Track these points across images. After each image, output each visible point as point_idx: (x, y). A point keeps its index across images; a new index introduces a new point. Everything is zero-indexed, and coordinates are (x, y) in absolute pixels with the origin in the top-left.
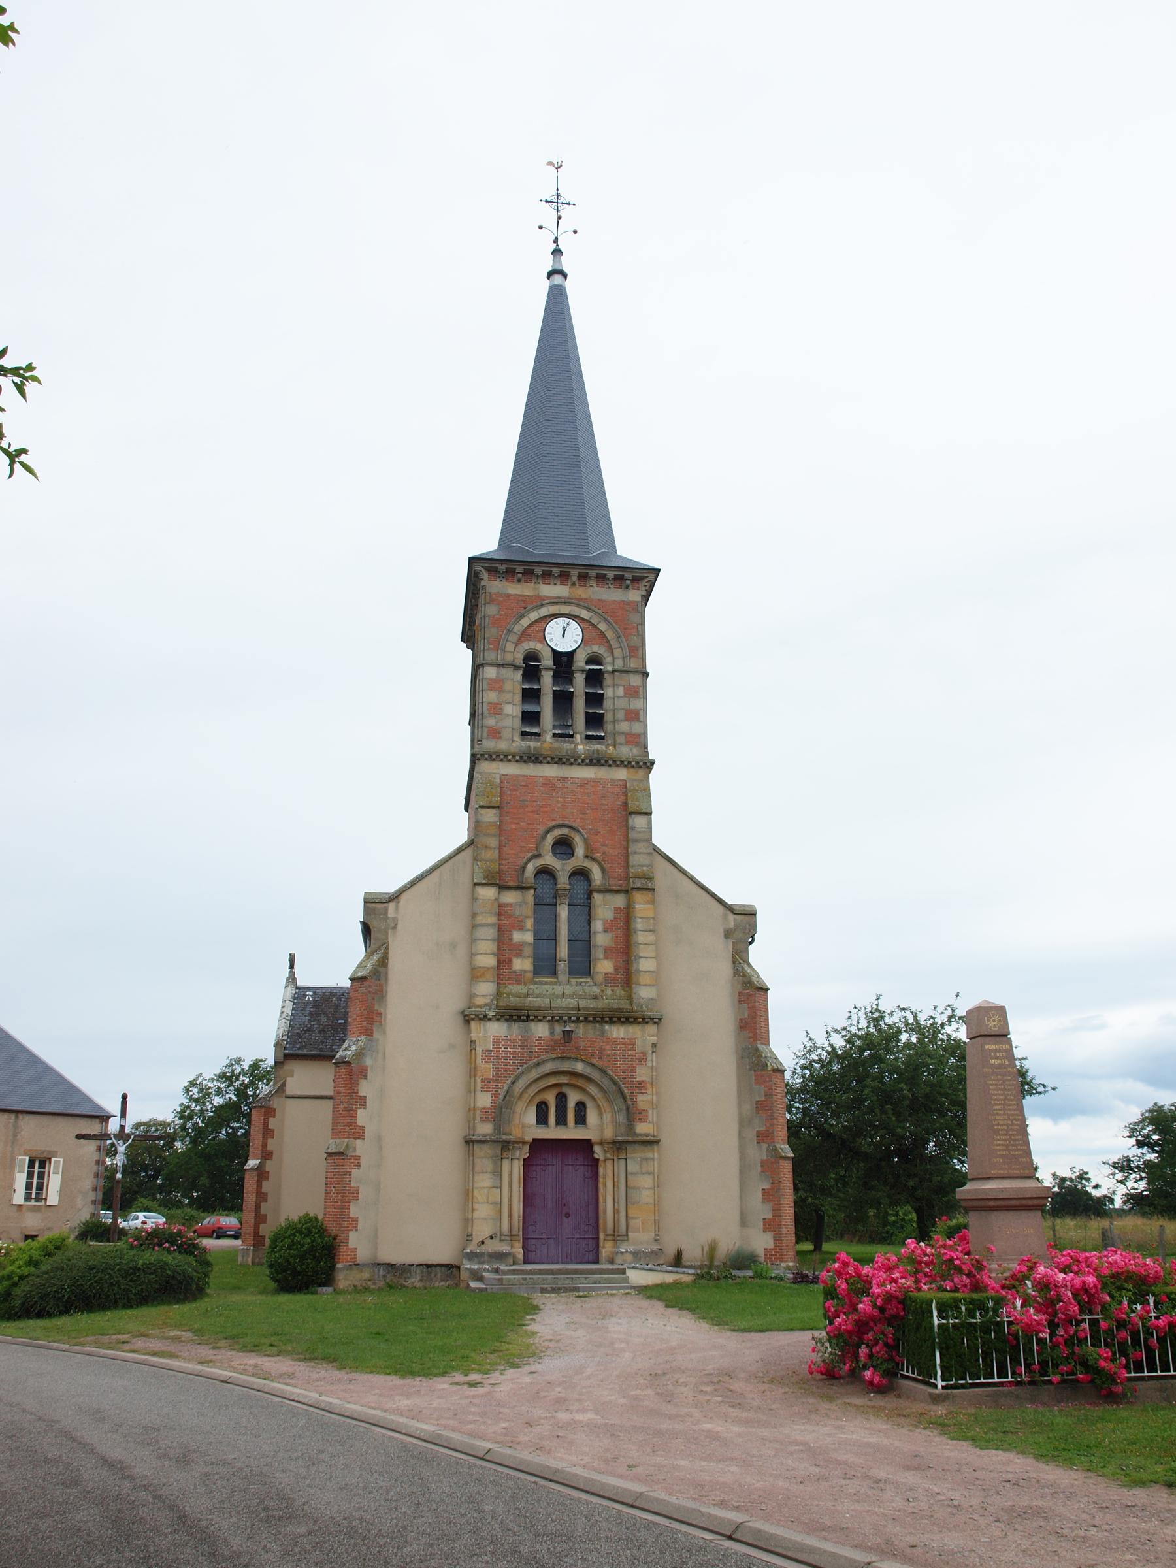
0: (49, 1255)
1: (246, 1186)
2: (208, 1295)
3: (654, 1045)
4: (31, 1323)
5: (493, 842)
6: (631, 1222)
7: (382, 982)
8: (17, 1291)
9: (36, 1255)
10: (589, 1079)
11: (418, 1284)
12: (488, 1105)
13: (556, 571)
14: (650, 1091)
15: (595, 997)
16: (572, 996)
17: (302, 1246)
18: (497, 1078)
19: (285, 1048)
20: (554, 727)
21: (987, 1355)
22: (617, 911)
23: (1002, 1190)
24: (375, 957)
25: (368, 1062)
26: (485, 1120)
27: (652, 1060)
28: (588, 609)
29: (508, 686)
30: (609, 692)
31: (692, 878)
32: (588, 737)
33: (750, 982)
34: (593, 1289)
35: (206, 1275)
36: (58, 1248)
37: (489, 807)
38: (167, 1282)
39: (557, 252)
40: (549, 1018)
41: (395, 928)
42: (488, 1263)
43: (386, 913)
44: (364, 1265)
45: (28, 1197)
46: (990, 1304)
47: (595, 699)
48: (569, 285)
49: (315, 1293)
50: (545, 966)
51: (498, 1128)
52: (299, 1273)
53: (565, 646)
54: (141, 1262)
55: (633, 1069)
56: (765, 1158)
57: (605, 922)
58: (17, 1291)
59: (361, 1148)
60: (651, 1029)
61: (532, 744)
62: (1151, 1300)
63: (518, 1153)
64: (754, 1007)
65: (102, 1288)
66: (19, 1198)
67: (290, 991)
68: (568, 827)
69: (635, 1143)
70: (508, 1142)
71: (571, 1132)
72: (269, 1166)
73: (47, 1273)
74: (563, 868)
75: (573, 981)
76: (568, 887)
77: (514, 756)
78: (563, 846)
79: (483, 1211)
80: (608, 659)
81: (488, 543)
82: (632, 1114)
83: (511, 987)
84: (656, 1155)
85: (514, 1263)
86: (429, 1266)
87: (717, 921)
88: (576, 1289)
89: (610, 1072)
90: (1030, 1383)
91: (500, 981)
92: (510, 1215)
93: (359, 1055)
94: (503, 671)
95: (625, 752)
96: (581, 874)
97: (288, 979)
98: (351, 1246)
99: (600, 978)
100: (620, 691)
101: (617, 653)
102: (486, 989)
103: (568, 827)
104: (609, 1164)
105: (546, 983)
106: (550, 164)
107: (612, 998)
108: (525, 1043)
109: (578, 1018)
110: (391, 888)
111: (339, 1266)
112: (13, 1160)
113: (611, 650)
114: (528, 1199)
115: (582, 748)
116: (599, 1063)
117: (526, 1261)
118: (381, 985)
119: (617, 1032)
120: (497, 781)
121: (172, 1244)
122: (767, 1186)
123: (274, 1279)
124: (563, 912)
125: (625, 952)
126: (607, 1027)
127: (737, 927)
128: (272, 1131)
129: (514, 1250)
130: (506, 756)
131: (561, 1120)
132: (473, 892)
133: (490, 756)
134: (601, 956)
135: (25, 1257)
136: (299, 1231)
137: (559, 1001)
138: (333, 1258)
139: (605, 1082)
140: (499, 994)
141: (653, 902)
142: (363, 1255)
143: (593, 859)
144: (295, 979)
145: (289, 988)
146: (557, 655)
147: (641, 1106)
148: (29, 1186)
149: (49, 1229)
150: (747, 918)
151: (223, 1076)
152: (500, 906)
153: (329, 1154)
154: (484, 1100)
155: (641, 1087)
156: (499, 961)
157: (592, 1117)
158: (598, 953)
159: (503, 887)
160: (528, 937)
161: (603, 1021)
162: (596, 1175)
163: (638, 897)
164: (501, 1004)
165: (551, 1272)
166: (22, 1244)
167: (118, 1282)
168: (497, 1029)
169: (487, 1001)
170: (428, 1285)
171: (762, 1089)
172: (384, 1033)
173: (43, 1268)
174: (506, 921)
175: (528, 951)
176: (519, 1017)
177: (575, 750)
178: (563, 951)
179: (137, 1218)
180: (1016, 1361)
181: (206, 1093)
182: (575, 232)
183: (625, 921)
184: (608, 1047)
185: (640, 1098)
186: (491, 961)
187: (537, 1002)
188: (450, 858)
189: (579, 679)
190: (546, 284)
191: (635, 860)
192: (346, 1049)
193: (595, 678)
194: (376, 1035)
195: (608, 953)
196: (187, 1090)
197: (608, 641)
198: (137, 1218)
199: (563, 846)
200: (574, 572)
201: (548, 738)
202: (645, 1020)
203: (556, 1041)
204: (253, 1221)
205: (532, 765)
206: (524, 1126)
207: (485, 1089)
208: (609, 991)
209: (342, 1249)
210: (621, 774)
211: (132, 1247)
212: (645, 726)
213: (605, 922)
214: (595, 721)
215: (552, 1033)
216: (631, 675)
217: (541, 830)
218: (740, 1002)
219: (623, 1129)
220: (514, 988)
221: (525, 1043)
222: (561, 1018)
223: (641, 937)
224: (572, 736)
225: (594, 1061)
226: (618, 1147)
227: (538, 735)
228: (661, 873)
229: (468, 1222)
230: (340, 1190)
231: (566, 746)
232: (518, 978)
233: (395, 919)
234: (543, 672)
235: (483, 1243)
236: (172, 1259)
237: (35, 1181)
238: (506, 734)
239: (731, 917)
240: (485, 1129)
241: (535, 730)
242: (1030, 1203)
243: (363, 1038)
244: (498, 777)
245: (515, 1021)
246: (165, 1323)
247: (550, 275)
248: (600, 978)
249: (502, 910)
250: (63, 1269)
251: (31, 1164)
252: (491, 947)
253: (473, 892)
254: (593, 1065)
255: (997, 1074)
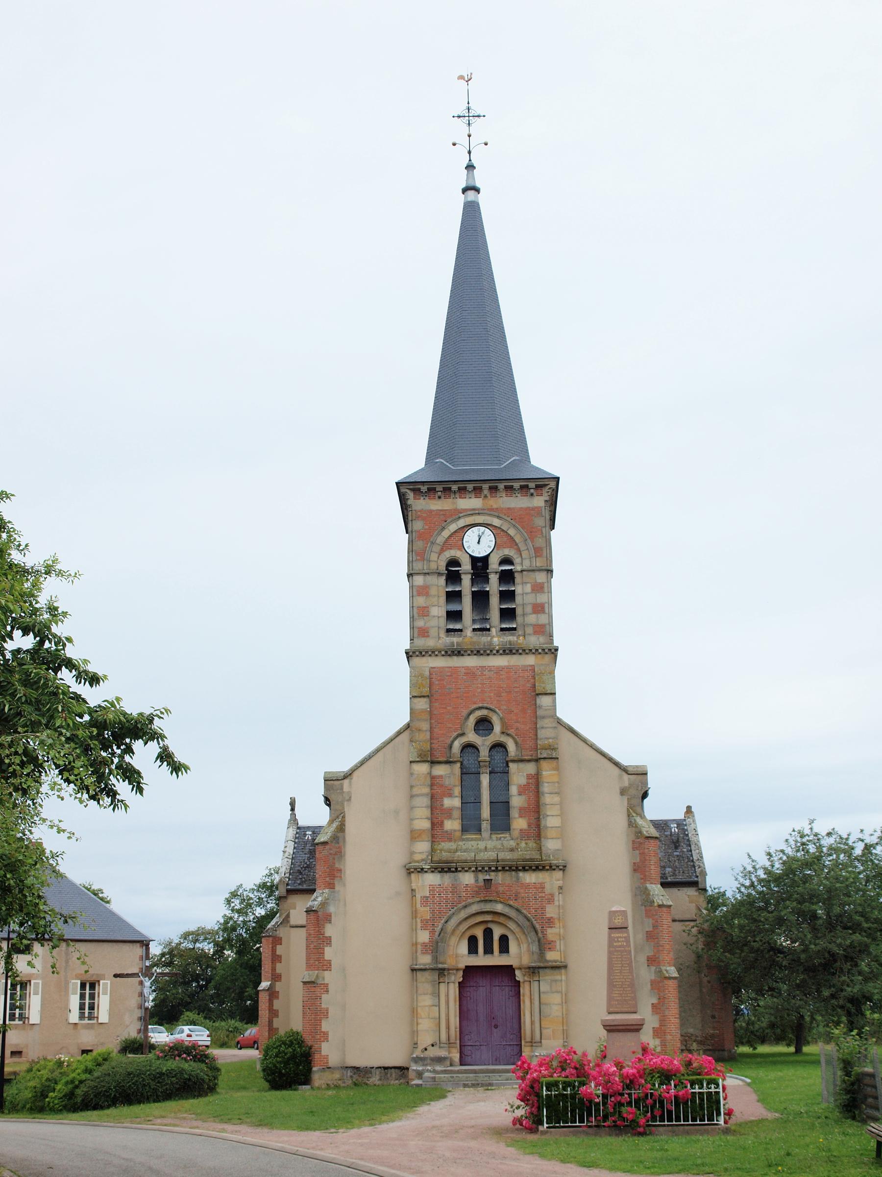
0: (99, 1065)
1: (260, 1005)
2: (218, 1093)
3: (561, 888)
4: (89, 1113)
5: (425, 726)
6: (544, 1031)
7: (341, 844)
8: (79, 1092)
9: (90, 1065)
10: (510, 918)
11: (378, 1083)
12: (427, 940)
13: (470, 487)
14: (557, 925)
15: (512, 850)
16: (492, 850)
17: (286, 1054)
18: (433, 919)
19: (287, 885)
20: (474, 621)
21: (573, 1111)
22: (529, 777)
23: (613, 1020)
24: (335, 825)
25: (332, 909)
26: (424, 953)
27: (559, 900)
28: (498, 517)
29: (433, 591)
30: (518, 589)
31: (592, 746)
32: (502, 630)
33: (640, 832)
34: (504, 1085)
35: (215, 1078)
36: (105, 1060)
37: (420, 697)
38: (185, 1083)
39: (470, 167)
40: (473, 869)
41: (349, 800)
42: (430, 1065)
43: (342, 789)
44: (335, 1068)
45: (82, 1017)
46: (577, 1084)
47: (507, 596)
48: (482, 199)
49: (295, 1090)
50: (471, 825)
51: (435, 959)
52: (284, 1075)
53: (480, 551)
54: (165, 1069)
55: (543, 908)
56: (653, 978)
57: (520, 786)
58: (79, 1092)
59: (328, 977)
60: (558, 874)
61: (455, 639)
62: (672, 1083)
63: (453, 978)
64: (643, 853)
65: (138, 1088)
66: (74, 1017)
67: (292, 832)
68: (487, 708)
69: (545, 968)
70: (444, 969)
71: (496, 959)
72: (278, 986)
73: (98, 1078)
74: (484, 743)
75: (494, 836)
76: (488, 759)
77: (440, 652)
78: (483, 725)
79: (425, 1024)
80: (517, 560)
81: (413, 461)
82: (543, 945)
83: (443, 844)
84: (564, 978)
85: (451, 1065)
86: (385, 1068)
87: (614, 780)
88: (490, 1085)
89: (524, 911)
90: (597, 1126)
91: (434, 839)
92: (448, 1028)
93: (324, 904)
94: (429, 578)
95: (534, 641)
96: (499, 746)
97: (290, 820)
98: (323, 1053)
99: (516, 834)
100: (528, 588)
101: (525, 554)
102: (423, 847)
103: (487, 708)
104: (527, 985)
105: (472, 840)
106: (461, 77)
107: (525, 850)
108: (455, 889)
109: (497, 868)
110: (345, 768)
111: (314, 1069)
112: (67, 983)
113: (519, 551)
114: (463, 1014)
115: (496, 639)
116: (516, 905)
117: (462, 1063)
118: (339, 847)
119: (529, 878)
120: (427, 673)
121: (189, 1055)
122: (655, 1001)
123: (266, 1080)
124: (485, 780)
125: (535, 811)
126: (521, 874)
127: (631, 785)
128: (280, 957)
129: (451, 1055)
130: (433, 652)
131: (488, 950)
132: (410, 769)
133: (421, 653)
134: (517, 815)
135: (83, 1067)
136: (284, 1043)
137: (482, 854)
138: (310, 1063)
139: (521, 919)
140: (433, 850)
141: (557, 769)
142: (334, 1060)
143: (508, 735)
144: (296, 820)
145: (291, 829)
146: (474, 560)
147: (550, 937)
148: (82, 1007)
149: (102, 1044)
150: (639, 777)
151: (263, 886)
152: (433, 778)
153: (305, 983)
154: (424, 937)
155: (550, 922)
156: (433, 824)
157: (513, 946)
158: (514, 813)
159: (433, 763)
160: (456, 802)
161: (517, 869)
162: (518, 994)
163: (544, 764)
164: (435, 859)
165: (475, 1072)
166: (80, 1058)
167: (148, 1084)
168: (432, 879)
169: (424, 856)
170: (385, 1083)
171: (651, 921)
172: (344, 885)
173: (96, 1074)
174: (438, 790)
175: (457, 814)
176: (449, 869)
177: (491, 643)
178: (486, 812)
179: (182, 1032)
180: (589, 1115)
181: (248, 905)
182: (486, 144)
183: (535, 784)
184: (522, 891)
185: (549, 931)
186: (426, 825)
187: (461, 855)
188: (391, 740)
189: (494, 579)
190: (461, 199)
191: (541, 734)
192: (315, 900)
193: (507, 577)
194: (337, 888)
195: (523, 812)
196: (228, 902)
197: (517, 545)
198: (182, 1032)
199: (483, 725)
200: (486, 486)
201: (469, 633)
202: (552, 868)
203: (479, 887)
204: (267, 1034)
205: (455, 658)
206: (457, 956)
207: (424, 928)
208: (523, 845)
209: (317, 1056)
210: (530, 660)
211: (158, 1058)
212: (550, 617)
213: (520, 786)
214: (508, 614)
215: (477, 880)
216: (537, 573)
217: (465, 712)
218: (634, 849)
219: (536, 957)
220: (446, 845)
221: (455, 889)
222: (483, 868)
223: (547, 799)
224: (489, 630)
225: (511, 903)
226: (533, 971)
227: (461, 630)
228: (566, 743)
229: (414, 1033)
230: (315, 1012)
231: (484, 639)
232: (449, 836)
233: (349, 793)
234: (463, 576)
235: (426, 1049)
236: (189, 1066)
237: (87, 1001)
238: (433, 632)
239: (626, 777)
240: (425, 960)
241: (458, 626)
242: (632, 1027)
243: (327, 890)
244: (427, 670)
245: (446, 872)
246: (179, 1110)
247: (464, 191)
248: (516, 834)
249: (434, 782)
250: (109, 1075)
251: (83, 986)
252: (427, 812)
253: (410, 769)
254: (510, 906)
255: (617, 951)
